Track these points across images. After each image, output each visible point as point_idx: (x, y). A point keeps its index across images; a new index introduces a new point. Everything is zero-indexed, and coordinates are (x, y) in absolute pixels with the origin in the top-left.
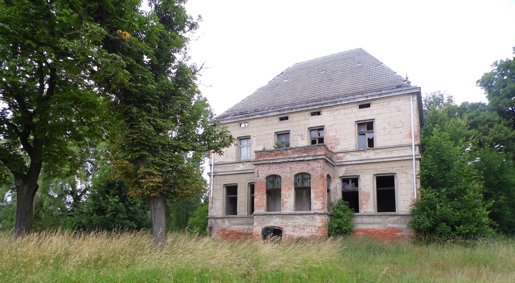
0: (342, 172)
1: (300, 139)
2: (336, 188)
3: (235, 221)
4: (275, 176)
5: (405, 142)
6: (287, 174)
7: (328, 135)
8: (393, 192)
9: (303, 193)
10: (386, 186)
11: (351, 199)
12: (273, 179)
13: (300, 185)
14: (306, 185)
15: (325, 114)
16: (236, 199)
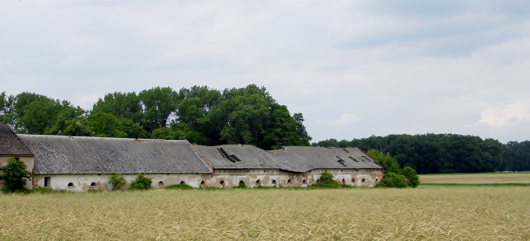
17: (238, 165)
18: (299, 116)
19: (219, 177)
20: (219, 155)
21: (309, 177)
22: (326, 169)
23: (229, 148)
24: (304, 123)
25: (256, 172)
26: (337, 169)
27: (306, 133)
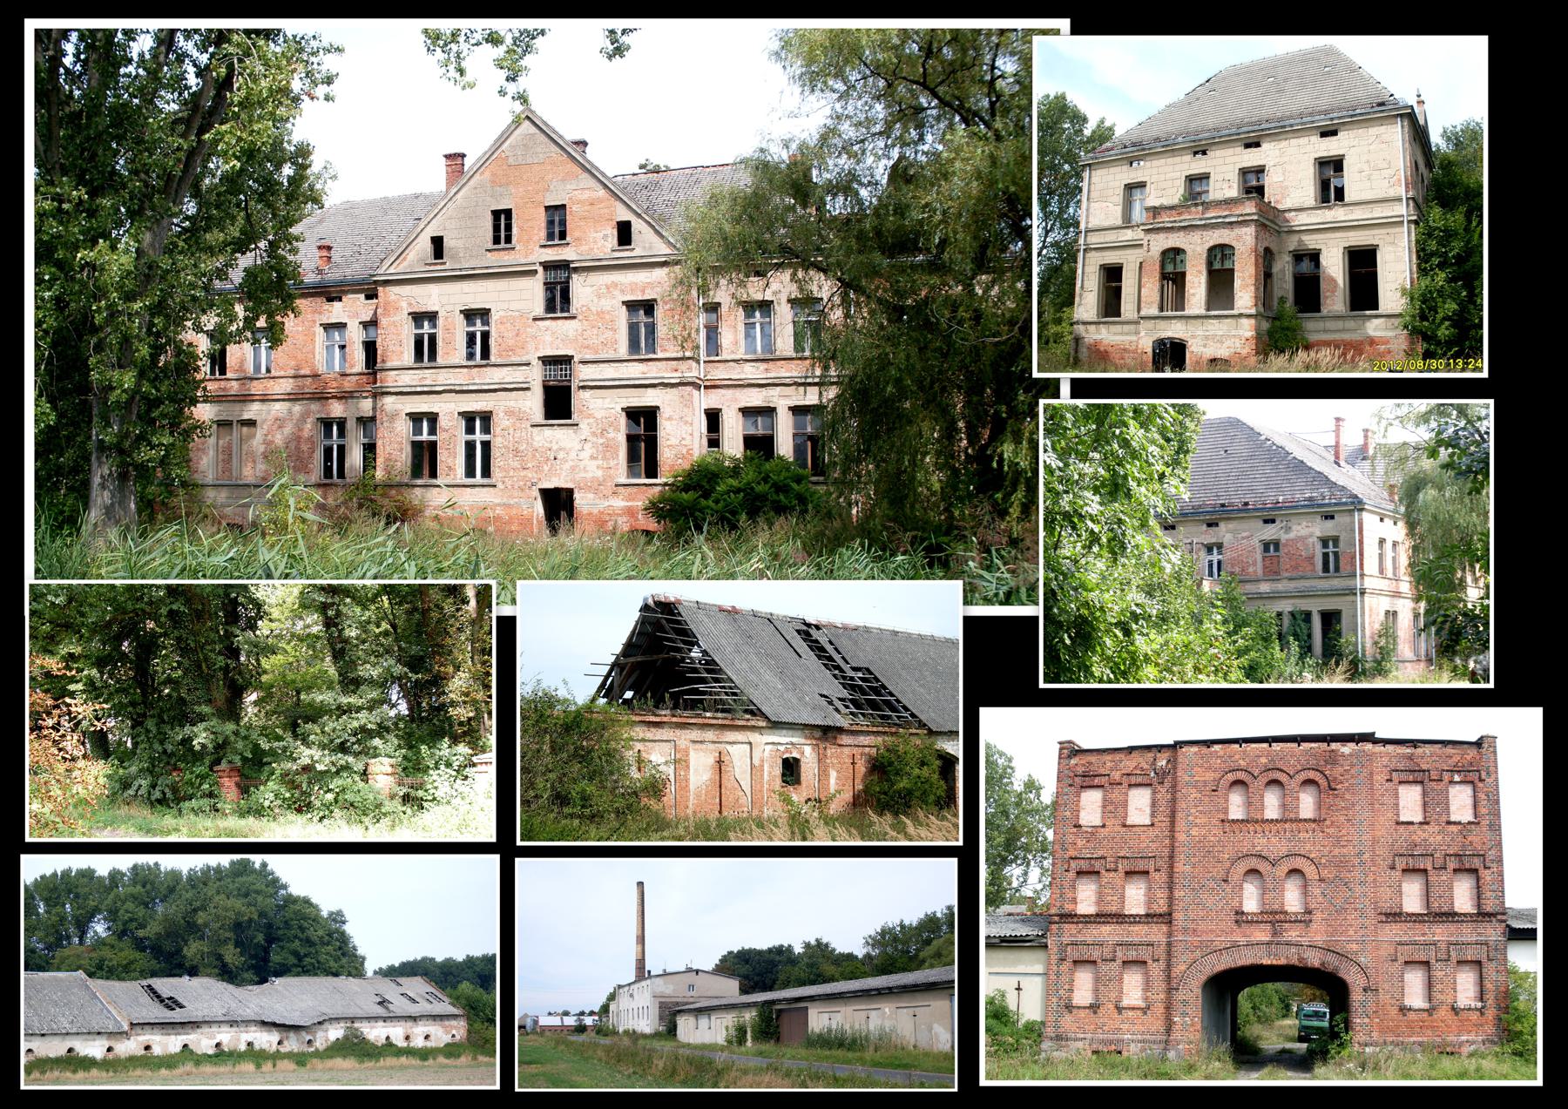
0: (1292, 243)
1: (1225, 185)
2: (1283, 271)
3: (1118, 328)
4: (1177, 251)
5: (1392, 193)
6: (1196, 246)
7: (1271, 182)
8: (1375, 274)
9: (1220, 281)
10: (1362, 263)
11: (1308, 290)
12: (1173, 255)
13: (1217, 266)
14: (1227, 265)
15: (1265, 146)
16: (1120, 288)
17: (176, 1015)
18: (338, 917)
19: (141, 1038)
20: (145, 999)
21: (320, 1034)
22: (353, 1020)
23: (165, 985)
24: (348, 928)
25: (215, 1029)
26: (376, 1018)
27: (355, 948)
